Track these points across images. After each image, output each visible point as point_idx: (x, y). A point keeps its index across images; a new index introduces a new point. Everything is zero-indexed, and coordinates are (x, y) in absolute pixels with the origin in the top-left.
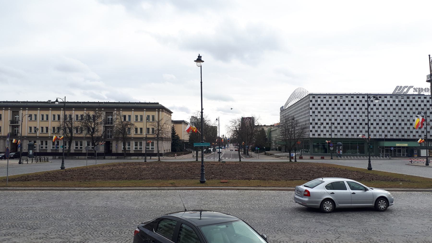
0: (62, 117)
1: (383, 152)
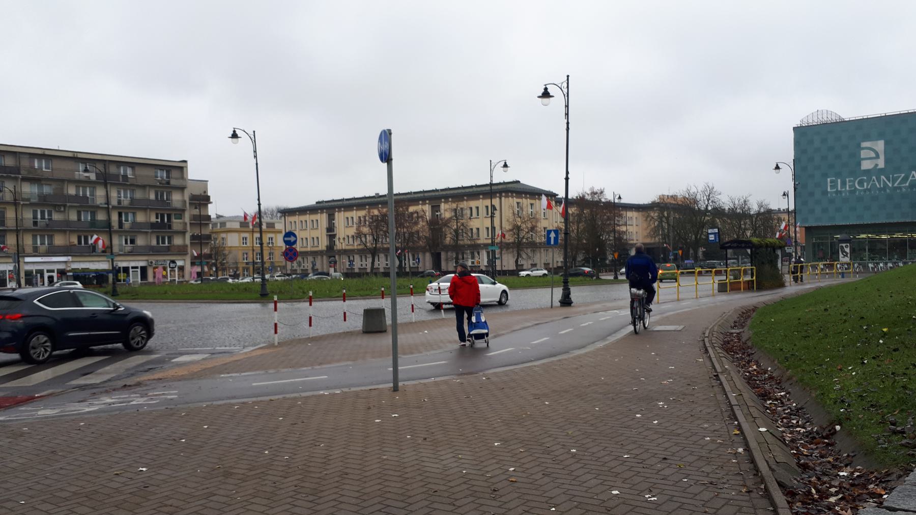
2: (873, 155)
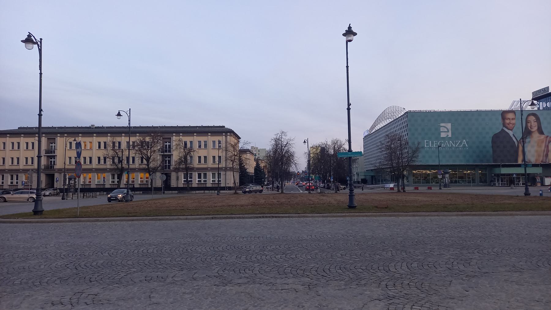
0: (223, 145)
1: (498, 180)
2: (446, 130)
